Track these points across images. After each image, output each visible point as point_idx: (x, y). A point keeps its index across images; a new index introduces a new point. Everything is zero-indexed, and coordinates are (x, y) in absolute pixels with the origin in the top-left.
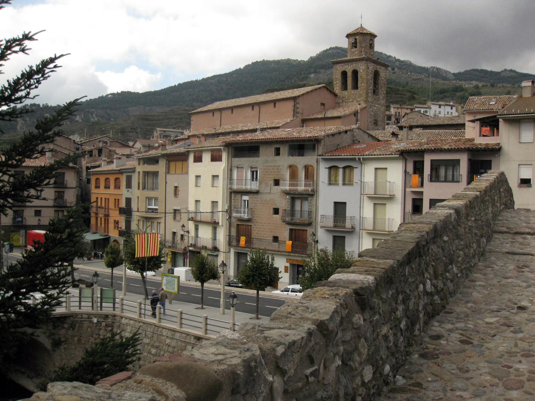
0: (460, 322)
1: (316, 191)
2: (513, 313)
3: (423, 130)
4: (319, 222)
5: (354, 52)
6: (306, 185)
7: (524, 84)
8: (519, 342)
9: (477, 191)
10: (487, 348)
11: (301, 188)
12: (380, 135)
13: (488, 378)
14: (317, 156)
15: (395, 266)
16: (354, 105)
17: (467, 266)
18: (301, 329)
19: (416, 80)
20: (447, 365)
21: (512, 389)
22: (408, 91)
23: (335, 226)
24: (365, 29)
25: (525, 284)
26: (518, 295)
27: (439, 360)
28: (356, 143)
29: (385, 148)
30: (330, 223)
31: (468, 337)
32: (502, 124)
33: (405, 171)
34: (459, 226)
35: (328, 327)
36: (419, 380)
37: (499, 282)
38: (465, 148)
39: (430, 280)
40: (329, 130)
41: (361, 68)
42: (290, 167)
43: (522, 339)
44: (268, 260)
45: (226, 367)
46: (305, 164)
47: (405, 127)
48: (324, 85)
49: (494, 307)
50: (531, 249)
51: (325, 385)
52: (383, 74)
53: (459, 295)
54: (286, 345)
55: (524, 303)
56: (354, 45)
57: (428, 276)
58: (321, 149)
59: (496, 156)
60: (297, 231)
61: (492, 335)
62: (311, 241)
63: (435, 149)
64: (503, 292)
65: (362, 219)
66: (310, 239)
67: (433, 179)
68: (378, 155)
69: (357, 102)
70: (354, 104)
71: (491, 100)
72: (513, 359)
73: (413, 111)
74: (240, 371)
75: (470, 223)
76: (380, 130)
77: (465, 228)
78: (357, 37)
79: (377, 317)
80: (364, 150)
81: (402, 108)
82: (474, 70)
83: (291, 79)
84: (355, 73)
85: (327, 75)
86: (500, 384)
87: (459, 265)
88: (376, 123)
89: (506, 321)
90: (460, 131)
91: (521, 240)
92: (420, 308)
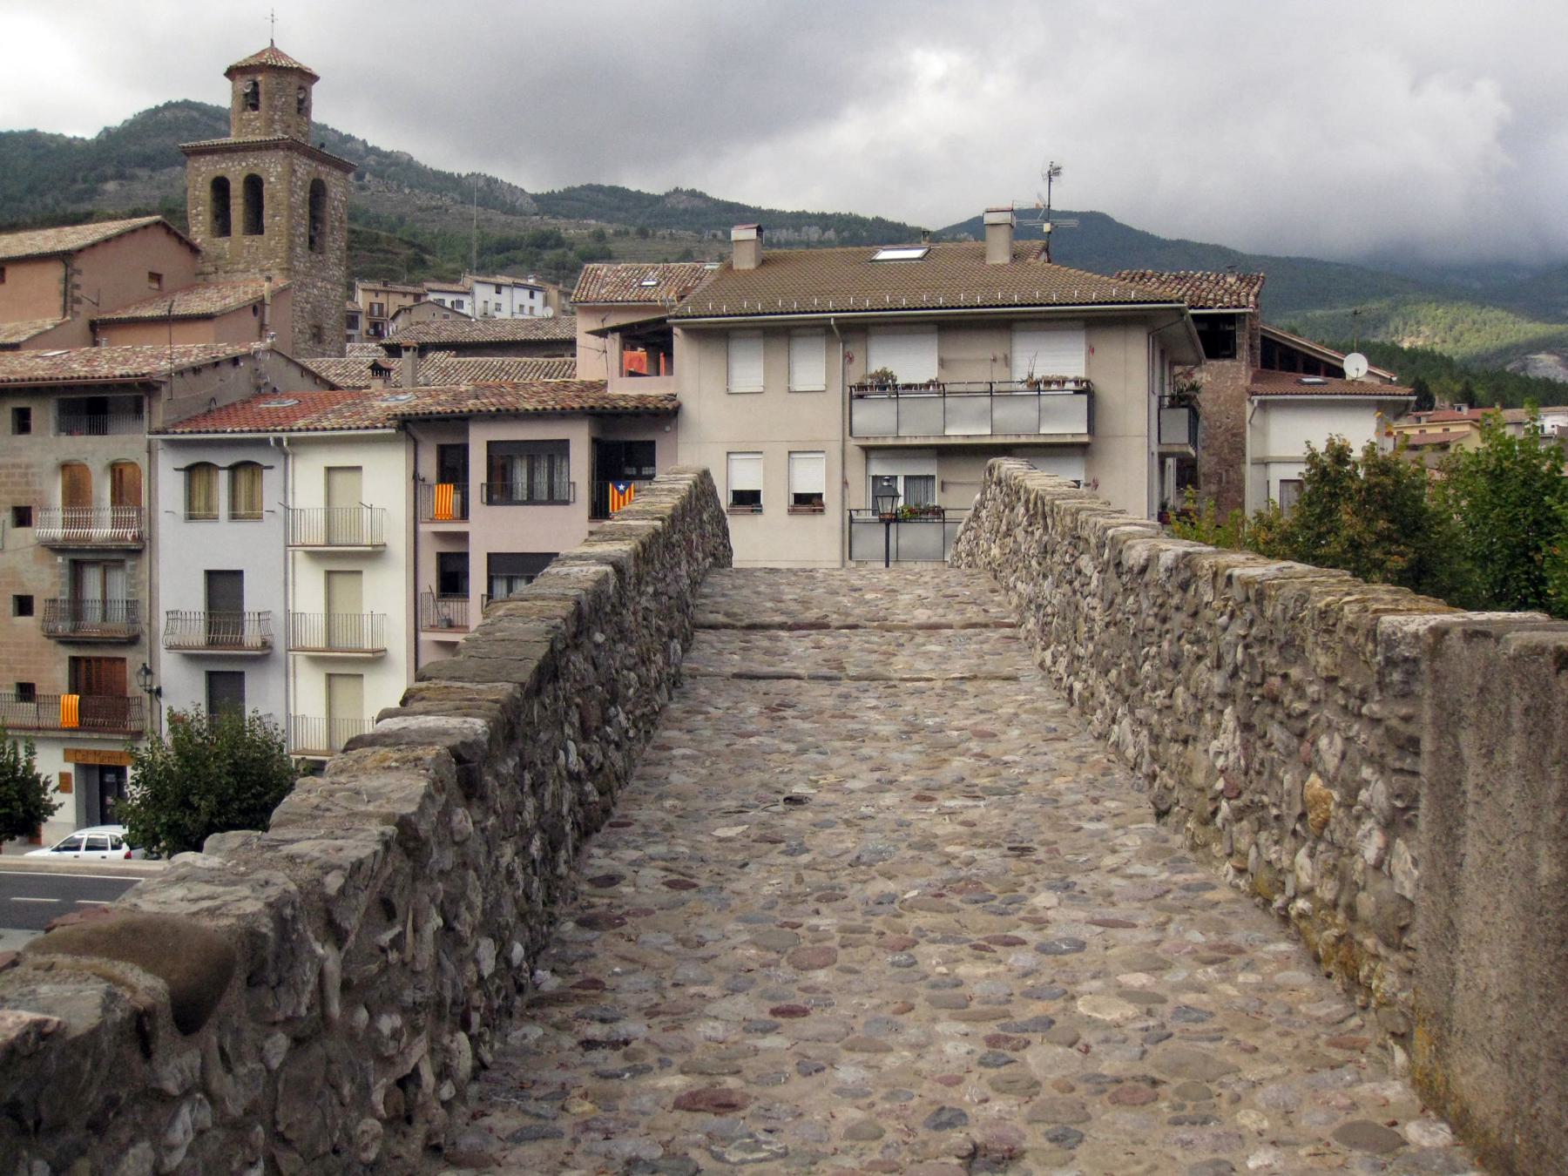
0: (655, 842)
1: (150, 540)
2: (778, 813)
3: (456, 356)
4: (161, 633)
5: (251, 120)
6: (116, 523)
7: (738, 233)
8: (806, 874)
9: (657, 519)
10: (733, 892)
11: (102, 531)
12: (332, 371)
13: (753, 951)
14: (150, 433)
15: (519, 696)
16: (252, 281)
17: (645, 710)
18: (362, 835)
19: (427, 209)
20: (649, 936)
21: (811, 967)
22: (407, 243)
23: (211, 643)
24: (284, 56)
25: (792, 747)
26: (782, 772)
27: (627, 929)
28: (265, 395)
29: (354, 410)
30: (197, 634)
31: (683, 875)
32: (680, 343)
33: (416, 478)
34: (624, 605)
35: (416, 830)
36: (592, 975)
37: (728, 745)
38: (582, 408)
39: (575, 742)
40: (184, 354)
41: (272, 169)
42: (65, 467)
43: (811, 866)
44: (16, 753)
45: (233, 920)
46: (114, 458)
47: (407, 349)
48: (158, 217)
49: (730, 803)
50: (794, 664)
51: (414, 973)
52: (338, 189)
53: (635, 784)
54: (345, 870)
55: (799, 789)
56: (251, 100)
57: (571, 732)
58: (159, 413)
59: (668, 429)
60: (93, 663)
61: (740, 863)
62: (140, 692)
63: (498, 410)
64: (744, 769)
65: (290, 618)
66: (134, 687)
67: (495, 497)
68: (333, 429)
69: (262, 271)
70: (251, 276)
71: (644, 275)
72: (800, 907)
73: (423, 299)
74: (266, 927)
75: (644, 602)
76: (330, 356)
77: (635, 613)
78: (260, 78)
79: (492, 820)
80: (291, 415)
81: (388, 292)
82: (590, 188)
83: (42, 194)
84: (254, 185)
85: (159, 188)
86: (784, 962)
87: (629, 707)
88: (318, 335)
89: (763, 832)
90: (562, 359)
91: (766, 643)
92: (565, 809)
